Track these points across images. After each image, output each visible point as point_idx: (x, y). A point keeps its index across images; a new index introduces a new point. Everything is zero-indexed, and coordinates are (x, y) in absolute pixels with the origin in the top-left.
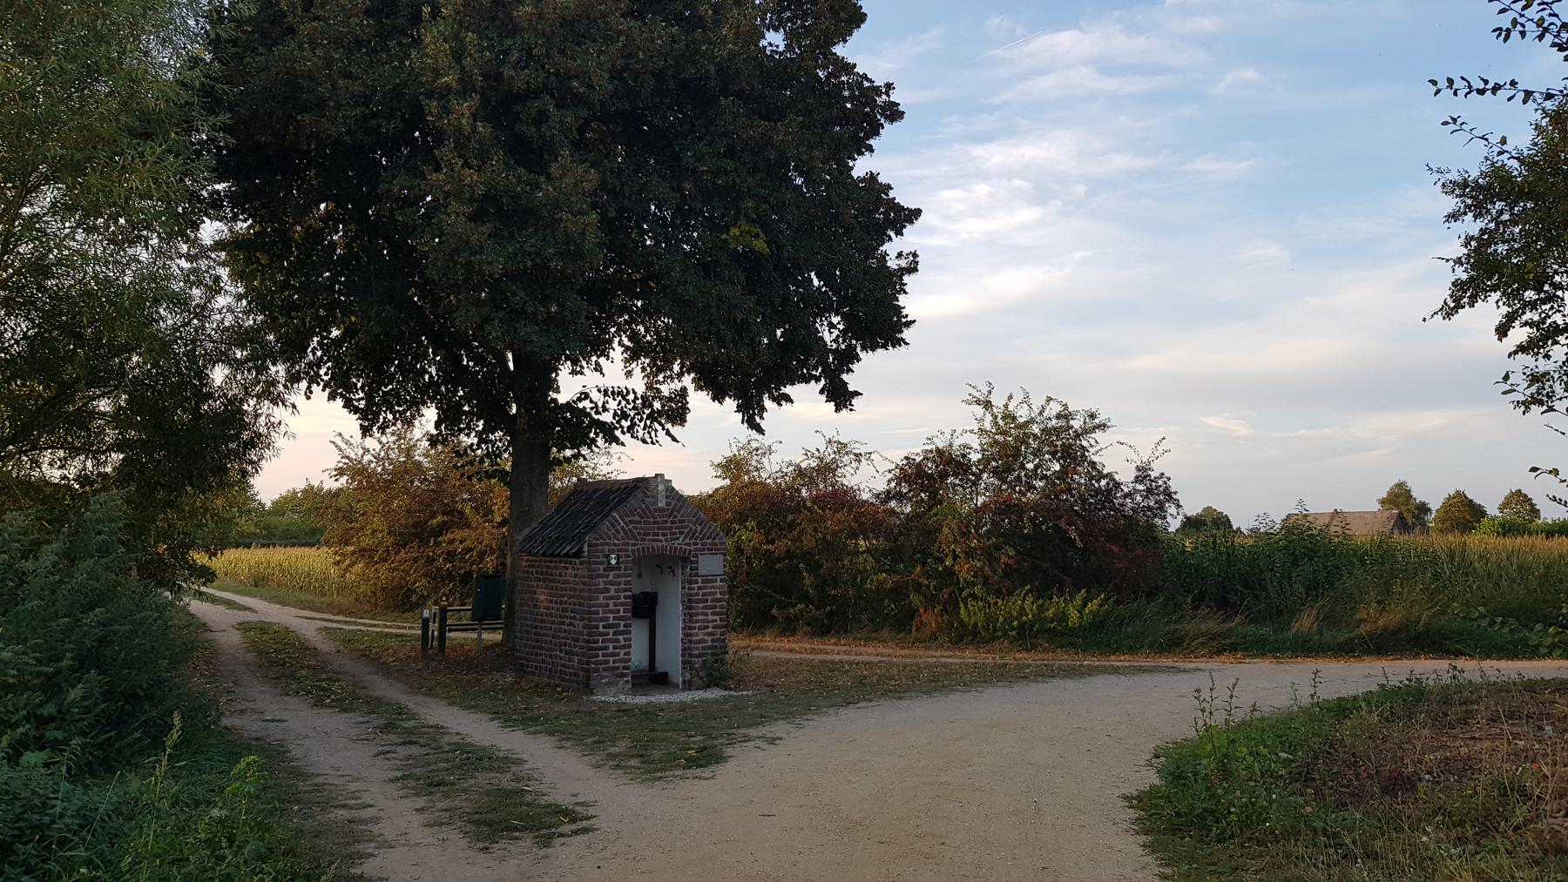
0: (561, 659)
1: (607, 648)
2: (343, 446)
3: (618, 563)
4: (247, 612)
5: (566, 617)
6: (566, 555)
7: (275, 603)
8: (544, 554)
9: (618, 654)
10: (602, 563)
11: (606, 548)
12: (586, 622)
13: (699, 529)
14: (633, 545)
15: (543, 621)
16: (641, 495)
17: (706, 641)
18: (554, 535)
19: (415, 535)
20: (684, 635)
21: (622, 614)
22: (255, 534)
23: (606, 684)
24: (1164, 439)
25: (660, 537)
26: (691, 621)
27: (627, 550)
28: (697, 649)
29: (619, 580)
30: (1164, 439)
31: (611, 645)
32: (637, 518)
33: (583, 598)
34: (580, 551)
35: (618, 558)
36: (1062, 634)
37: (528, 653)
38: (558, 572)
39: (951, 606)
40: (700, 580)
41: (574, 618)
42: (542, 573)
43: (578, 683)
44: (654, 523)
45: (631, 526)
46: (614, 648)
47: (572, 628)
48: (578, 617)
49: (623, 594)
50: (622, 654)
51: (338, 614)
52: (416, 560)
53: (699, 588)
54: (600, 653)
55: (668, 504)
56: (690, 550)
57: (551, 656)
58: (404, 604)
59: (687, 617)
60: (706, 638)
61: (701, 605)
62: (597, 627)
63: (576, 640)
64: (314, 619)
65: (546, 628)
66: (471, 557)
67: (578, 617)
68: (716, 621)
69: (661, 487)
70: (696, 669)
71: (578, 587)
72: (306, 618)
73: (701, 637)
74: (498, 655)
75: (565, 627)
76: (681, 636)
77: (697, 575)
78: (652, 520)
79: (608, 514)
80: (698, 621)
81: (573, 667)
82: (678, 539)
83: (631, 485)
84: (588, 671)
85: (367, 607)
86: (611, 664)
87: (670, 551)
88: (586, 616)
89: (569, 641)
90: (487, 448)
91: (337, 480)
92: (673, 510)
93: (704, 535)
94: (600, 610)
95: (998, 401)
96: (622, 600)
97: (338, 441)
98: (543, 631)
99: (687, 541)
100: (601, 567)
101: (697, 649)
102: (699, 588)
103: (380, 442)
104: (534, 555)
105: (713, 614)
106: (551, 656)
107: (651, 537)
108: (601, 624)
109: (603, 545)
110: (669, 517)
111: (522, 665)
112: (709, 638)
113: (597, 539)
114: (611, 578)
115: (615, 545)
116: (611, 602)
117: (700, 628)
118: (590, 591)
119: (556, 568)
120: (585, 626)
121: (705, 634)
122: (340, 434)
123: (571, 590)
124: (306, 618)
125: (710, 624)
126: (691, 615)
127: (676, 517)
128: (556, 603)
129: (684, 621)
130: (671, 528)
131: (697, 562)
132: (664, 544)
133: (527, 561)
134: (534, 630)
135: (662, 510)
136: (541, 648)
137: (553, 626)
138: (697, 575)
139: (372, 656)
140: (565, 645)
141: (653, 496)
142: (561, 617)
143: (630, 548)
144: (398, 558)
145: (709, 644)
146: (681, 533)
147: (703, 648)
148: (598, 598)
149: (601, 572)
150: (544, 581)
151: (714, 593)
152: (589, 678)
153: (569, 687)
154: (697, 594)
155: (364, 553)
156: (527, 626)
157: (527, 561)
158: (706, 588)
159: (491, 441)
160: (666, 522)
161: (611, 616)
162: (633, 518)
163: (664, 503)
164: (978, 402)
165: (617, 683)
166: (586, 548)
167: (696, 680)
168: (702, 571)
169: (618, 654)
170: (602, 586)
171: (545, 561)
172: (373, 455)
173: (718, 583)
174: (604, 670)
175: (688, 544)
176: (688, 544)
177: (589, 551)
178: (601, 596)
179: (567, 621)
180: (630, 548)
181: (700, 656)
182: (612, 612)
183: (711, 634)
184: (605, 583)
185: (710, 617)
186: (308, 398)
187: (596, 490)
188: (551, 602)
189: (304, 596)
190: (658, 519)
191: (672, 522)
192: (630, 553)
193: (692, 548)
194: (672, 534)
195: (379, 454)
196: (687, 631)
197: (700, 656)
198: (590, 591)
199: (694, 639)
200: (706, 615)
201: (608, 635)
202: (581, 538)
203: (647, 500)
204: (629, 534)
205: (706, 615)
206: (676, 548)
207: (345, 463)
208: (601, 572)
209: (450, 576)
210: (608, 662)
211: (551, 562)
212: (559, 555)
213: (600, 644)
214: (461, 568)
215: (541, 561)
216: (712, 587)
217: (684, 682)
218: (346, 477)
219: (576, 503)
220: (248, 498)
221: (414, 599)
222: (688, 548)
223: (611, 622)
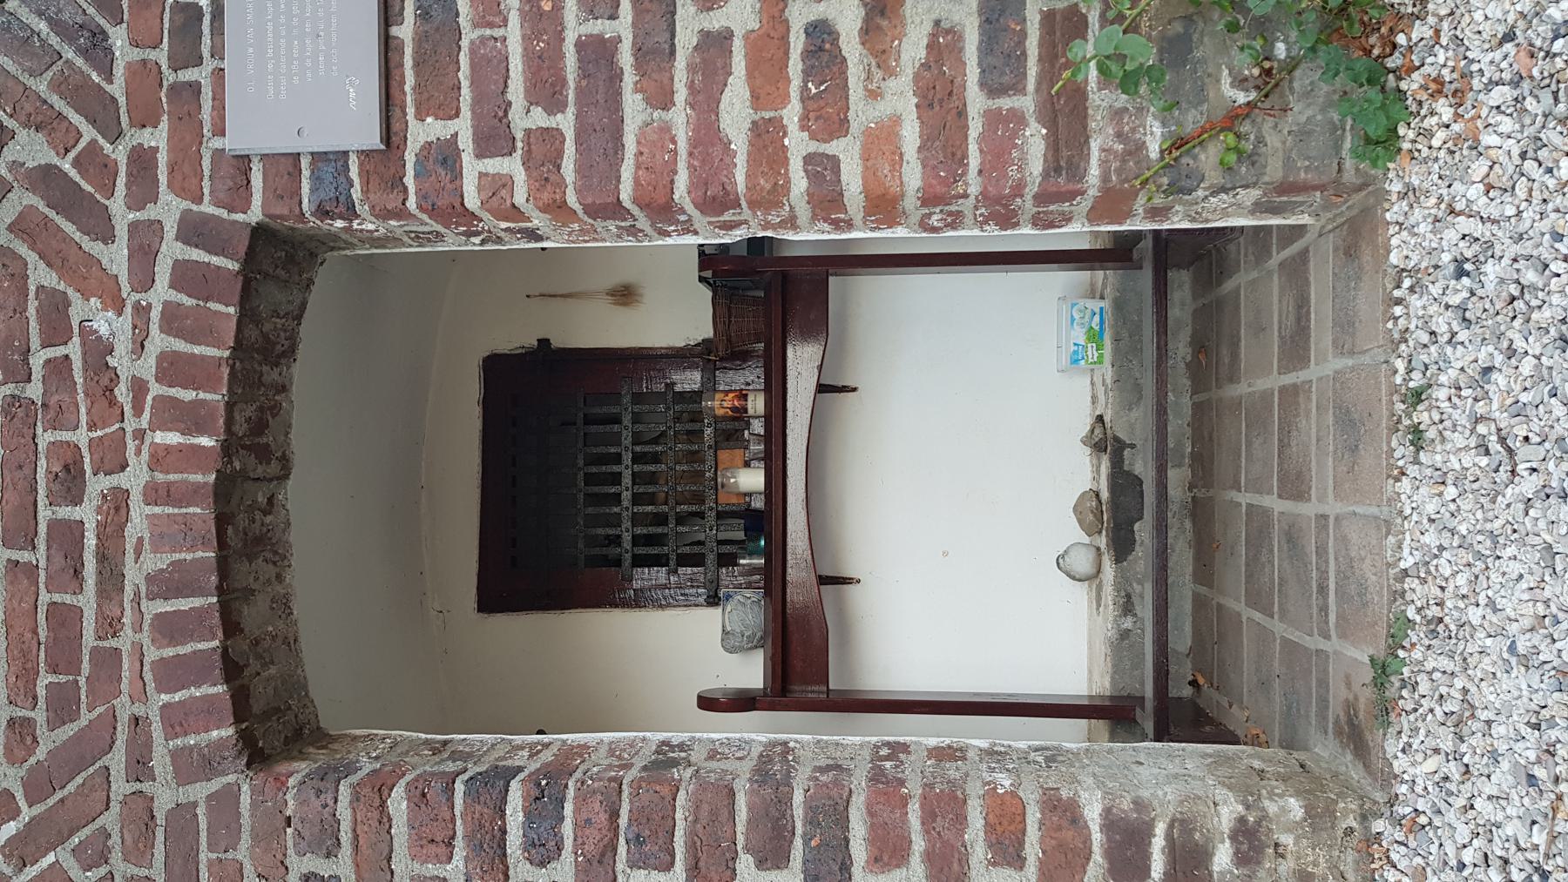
14: (140, 767)
25: (87, 514)
61: (634, 107)
82: (98, 351)
99: (116, 257)
102: (494, 138)
131: (285, 165)
192: (200, 791)
206: (172, 367)
222: (172, 250)
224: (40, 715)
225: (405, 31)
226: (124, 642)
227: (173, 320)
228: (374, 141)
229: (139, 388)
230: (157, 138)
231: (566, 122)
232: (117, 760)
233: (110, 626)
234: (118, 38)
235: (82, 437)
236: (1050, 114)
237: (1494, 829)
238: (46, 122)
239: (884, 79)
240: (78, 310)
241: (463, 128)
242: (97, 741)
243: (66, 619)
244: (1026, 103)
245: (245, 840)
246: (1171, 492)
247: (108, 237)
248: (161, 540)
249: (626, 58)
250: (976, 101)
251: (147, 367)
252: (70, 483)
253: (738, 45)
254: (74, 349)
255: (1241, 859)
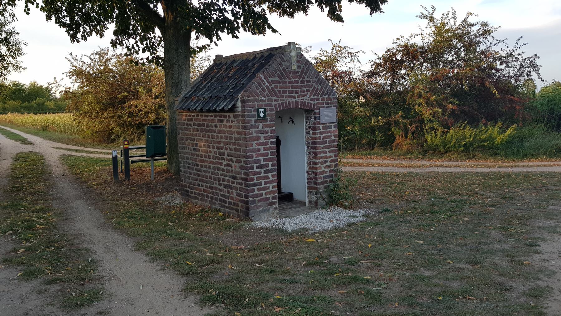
0: (220, 190)
1: (260, 184)
2: (73, 61)
3: (265, 116)
4: (29, 146)
5: (223, 159)
6: (223, 110)
7: (47, 139)
8: (201, 110)
9: (268, 188)
10: (253, 116)
11: (256, 103)
12: (242, 164)
13: (320, 87)
14: (276, 100)
15: (202, 161)
16: (279, 60)
17: (326, 172)
18: (207, 96)
19: (111, 104)
20: (310, 168)
21: (269, 156)
22: (54, 109)
23: (260, 212)
24: (521, 37)
25: (294, 94)
26: (316, 158)
27: (271, 105)
28: (321, 178)
29: (266, 129)
30: (521, 37)
31: (263, 181)
32: (277, 79)
33: (239, 145)
34: (234, 107)
35: (265, 111)
36: (490, 148)
37: (191, 183)
38: (213, 124)
39: (419, 132)
40: (321, 126)
41: (231, 160)
42: (199, 125)
43: (237, 210)
44: (290, 83)
45: (273, 86)
46: (266, 183)
47: (229, 168)
48: (234, 159)
49: (269, 141)
50: (271, 187)
51: (76, 145)
52: (112, 117)
53: (321, 133)
54: (255, 188)
55: (299, 67)
56: (314, 104)
57: (211, 188)
58: (108, 139)
59: (312, 155)
60: (326, 170)
61: (322, 146)
62: (252, 168)
63: (235, 178)
64: (61, 149)
65: (206, 167)
66: (141, 114)
67: (234, 159)
68: (332, 157)
69: (293, 53)
70: (320, 193)
71: (233, 136)
72: (57, 148)
73: (323, 169)
74: (166, 179)
75: (223, 167)
76: (307, 169)
77: (319, 123)
78: (288, 80)
79: (254, 75)
80: (320, 158)
81: (232, 198)
82: (306, 95)
83: (266, 54)
84: (247, 203)
85: (90, 141)
86: (264, 196)
87: (301, 105)
88: (243, 160)
89: (228, 178)
90: (147, 44)
91: (70, 78)
92: (302, 72)
93: (323, 93)
94: (254, 154)
95: (437, 16)
96: (270, 145)
97: (70, 57)
98: (203, 169)
99: (312, 97)
100: (253, 119)
101: (321, 178)
102: (321, 133)
103: (91, 59)
104: (192, 111)
105: (330, 152)
106: (211, 188)
107: (287, 94)
108: (255, 165)
109: (253, 101)
110: (300, 77)
111: (187, 191)
112: (327, 170)
113: (248, 97)
114: (260, 128)
115: (262, 101)
116: (261, 147)
117: (322, 163)
118: (245, 139)
119: (212, 121)
120: (241, 167)
121: (325, 167)
122: (71, 54)
123: (226, 138)
124: (57, 148)
125: (328, 160)
126: (315, 154)
127: (304, 78)
128: (213, 148)
129: (309, 158)
130: (301, 87)
131: (319, 113)
132: (297, 99)
133: (186, 116)
134: (195, 167)
135: (294, 72)
136: (203, 181)
137: (212, 166)
138: (319, 123)
139: (83, 180)
140: (224, 180)
141: (288, 61)
142: (219, 159)
143: (273, 103)
144: (103, 117)
145: (328, 174)
146: (308, 91)
147: (325, 177)
148: (252, 145)
149: (253, 123)
150: (202, 131)
151: (330, 136)
152: (248, 209)
153: (229, 213)
154: (320, 138)
155: (87, 114)
156: (189, 164)
157: (186, 116)
158: (325, 133)
159: (149, 38)
160: (297, 82)
161: (262, 158)
162: (274, 79)
163: (296, 67)
164: (426, 17)
165: (268, 211)
166: (239, 104)
167: (320, 201)
168: (323, 120)
169: (268, 188)
170: (254, 135)
171: (202, 116)
172: (87, 65)
173: (333, 129)
174: (259, 201)
175: (313, 100)
176: (313, 100)
177: (243, 107)
178: (254, 143)
179: (225, 162)
180: (273, 103)
181: (322, 183)
182: (262, 155)
183: (329, 167)
184: (256, 132)
185: (328, 154)
186: (28, 14)
187: (234, 61)
188: (209, 147)
189: (60, 135)
190: (292, 80)
191: (302, 82)
192: (274, 107)
193: (316, 102)
194: (302, 91)
195: (90, 65)
196: (312, 165)
197: (322, 183)
198: (245, 139)
199: (318, 171)
200: (326, 153)
201: (260, 173)
202: (233, 97)
203: (283, 63)
204: (272, 92)
205: (326, 153)
206: (305, 102)
207: (74, 70)
208: (253, 123)
209: (131, 125)
210: (261, 195)
211: (207, 116)
212: (215, 111)
213: (255, 181)
214: (136, 121)
215: (198, 116)
216: (329, 132)
217: (310, 202)
218: (75, 77)
219: (219, 72)
220: (50, 95)
221: (113, 137)
222: (313, 102)
223: (262, 163)
224: (278, 89)
225: (327, 125)
226: (285, 99)
227: (308, 103)
228: (321, 123)
229: (303, 99)
230: (320, 101)
231: (322, 140)
232: (275, 98)
233: (286, 97)
234: (327, 96)
235: (300, 94)
236: (322, 182)
237: (131, 48)
238: (321, 89)
239: (524, 124)
240: (309, 93)
241: (321, 130)
242: (277, 96)
243: (285, 92)
244: (323, 180)
245: (270, 112)
246: (138, 163)
247: (314, 96)
248: (293, 102)
249: (326, 145)
250: (323, 176)
251: (305, 100)
252: (296, 92)
253: (325, 155)
254: (306, 93)
255: (274, 208)
